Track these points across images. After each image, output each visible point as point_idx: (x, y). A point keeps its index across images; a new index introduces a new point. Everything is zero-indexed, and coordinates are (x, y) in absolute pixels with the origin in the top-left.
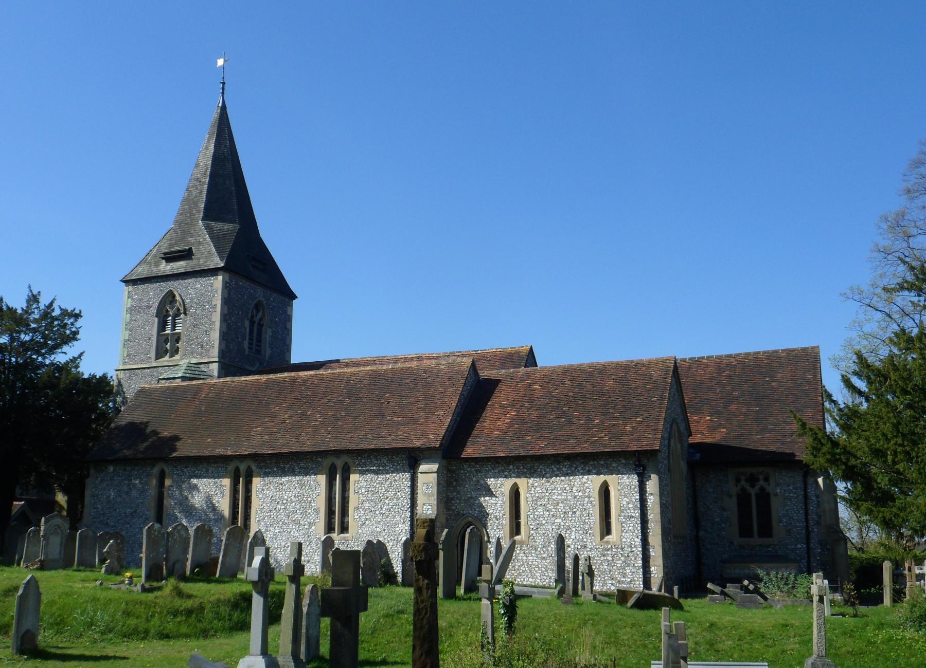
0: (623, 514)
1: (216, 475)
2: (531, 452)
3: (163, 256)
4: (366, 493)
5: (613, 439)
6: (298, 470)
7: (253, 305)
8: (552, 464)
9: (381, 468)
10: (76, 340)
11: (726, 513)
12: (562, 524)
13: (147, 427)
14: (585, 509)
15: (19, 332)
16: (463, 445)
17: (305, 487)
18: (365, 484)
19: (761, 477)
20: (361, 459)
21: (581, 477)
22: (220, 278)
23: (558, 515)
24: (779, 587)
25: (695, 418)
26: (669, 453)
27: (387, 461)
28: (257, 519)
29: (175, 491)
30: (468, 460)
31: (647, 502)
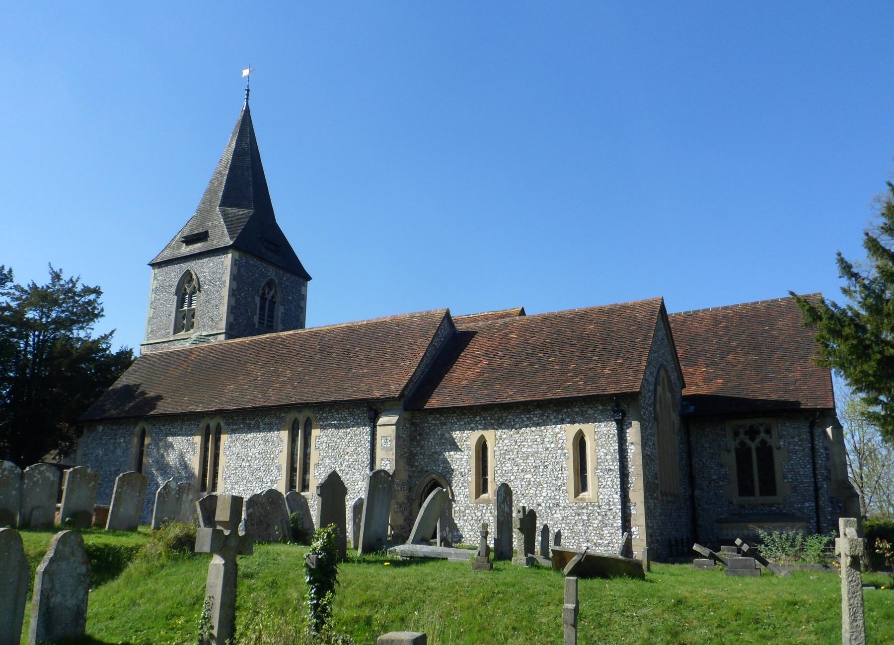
0: (600, 467)
2: (498, 400)
5: (589, 383)
7: (264, 283)
8: (521, 413)
10: (102, 316)
11: (724, 470)
12: (533, 479)
13: (138, 388)
14: (558, 463)
16: (428, 395)
18: (326, 439)
19: (762, 429)
20: (322, 414)
21: (553, 426)
22: (230, 255)
23: (528, 470)
24: (784, 550)
26: (655, 399)
28: (224, 477)
29: (153, 449)
30: (433, 411)
31: (628, 452)
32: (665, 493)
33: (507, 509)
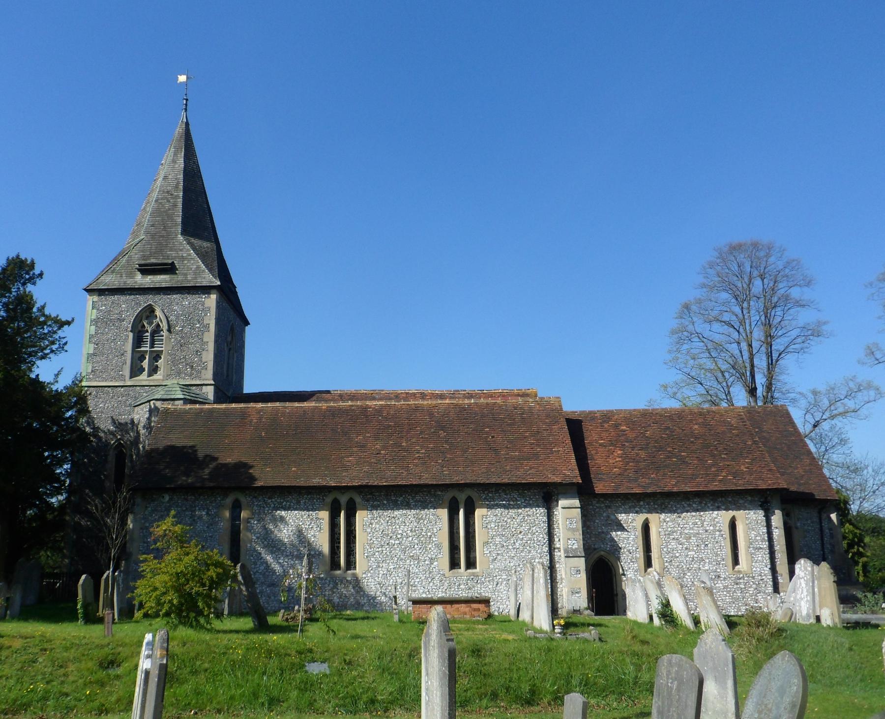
0: (751, 546)
1: (310, 507)
4: (496, 528)
6: (414, 503)
9: (512, 503)
14: (717, 542)
17: (424, 521)
21: (711, 512)
22: (214, 297)
27: (518, 495)
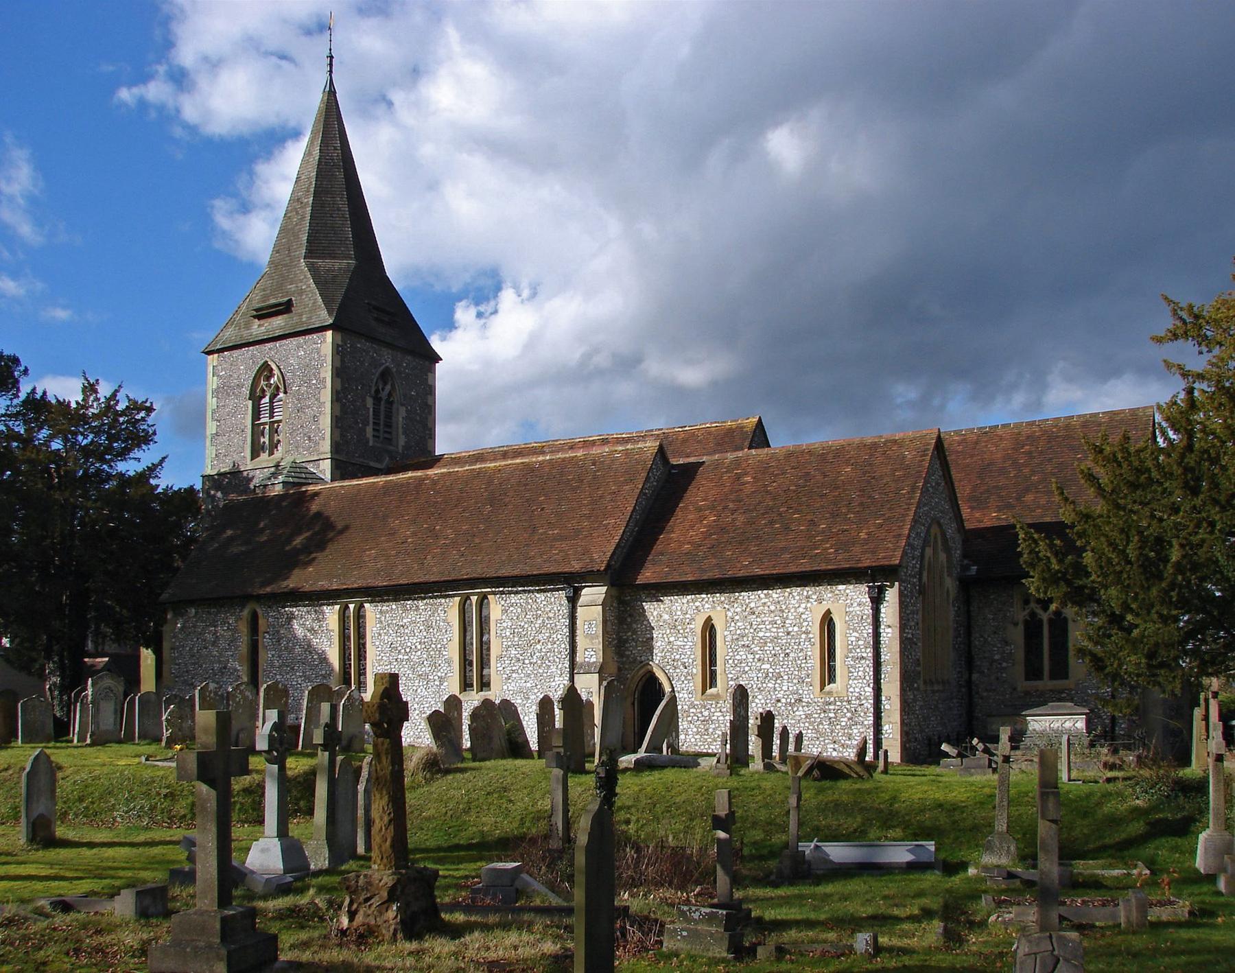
0: (850, 655)
2: (730, 573)
3: (255, 313)
6: (423, 607)
7: (377, 374)
11: (1008, 648)
12: (771, 670)
15: (75, 434)
18: (510, 624)
25: (977, 515)
30: (646, 587)
32: (930, 680)
33: (743, 712)
